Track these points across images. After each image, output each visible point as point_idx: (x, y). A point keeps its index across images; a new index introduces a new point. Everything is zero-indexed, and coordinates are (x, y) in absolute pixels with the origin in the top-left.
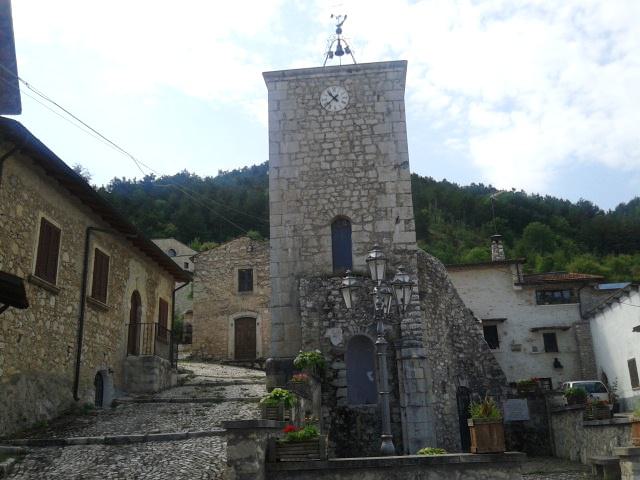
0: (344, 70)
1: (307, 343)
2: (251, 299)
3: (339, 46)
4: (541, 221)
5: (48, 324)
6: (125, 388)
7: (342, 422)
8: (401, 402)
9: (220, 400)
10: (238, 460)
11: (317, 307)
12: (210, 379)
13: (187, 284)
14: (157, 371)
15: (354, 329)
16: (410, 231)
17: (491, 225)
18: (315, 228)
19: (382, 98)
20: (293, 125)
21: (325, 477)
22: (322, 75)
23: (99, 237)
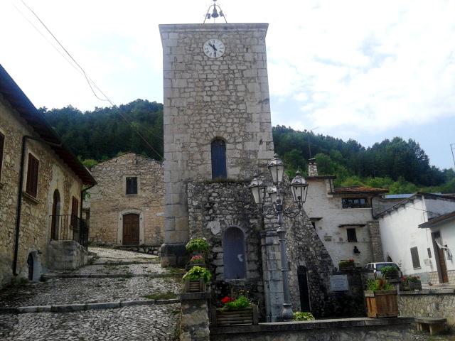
0: (221, 27)
2: (136, 200)
3: (215, 10)
4: (323, 152)
6: (50, 266)
7: (219, 292)
8: (265, 278)
9: (130, 276)
10: (193, 326)
12: (112, 260)
14: (75, 253)
15: (229, 221)
16: (270, 150)
17: (290, 154)
18: (199, 145)
19: (249, 50)
21: (258, 339)
22: (205, 30)
23: (32, 145)
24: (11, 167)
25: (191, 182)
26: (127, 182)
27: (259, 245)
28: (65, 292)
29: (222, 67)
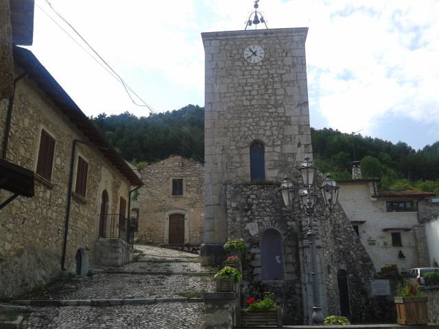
0: (261, 33)
1: (231, 233)
3: (256, 17)
4: (372, 155)
5: (45, 210)
6: (97, 262)
7: (257, 293)
8: (303, 280)
9: (169, 274)
11: (239, 207)
12: (157, 257)
13: (140, 187)
14: (120, 250)
15: (267, 222)
16: (309, 153)
17: (338, 156)
18: (238, 148)
24: (61, 169)
25: (230, 184)
26: (173, 184)
28: (107, 287)
29: (261, 72)
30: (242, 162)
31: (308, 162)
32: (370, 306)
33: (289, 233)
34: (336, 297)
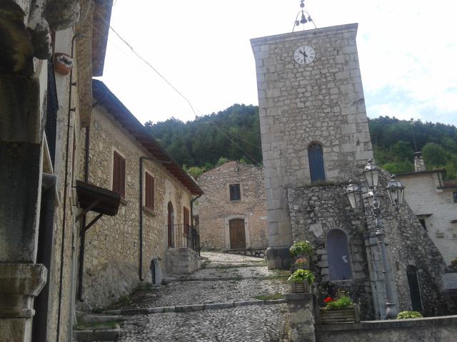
3: (303, 16)
4: (434, 141)
6: (169, 271)
8: (372, 279)
9: (240, 278)
13: (200, 195)
14: (190, 258)
15: (331, 223)
17: (397, 146)
18: (296, 151)
19: (340, 52)
20: (275, 77)
22: (294, 38)
27: (363, 246)
28: (185, 294)
29: (314, 73)
30: (301, 164)
31: (371, 165)
32: (442, 300)
33: (354, 232)
34: (406, 291)
